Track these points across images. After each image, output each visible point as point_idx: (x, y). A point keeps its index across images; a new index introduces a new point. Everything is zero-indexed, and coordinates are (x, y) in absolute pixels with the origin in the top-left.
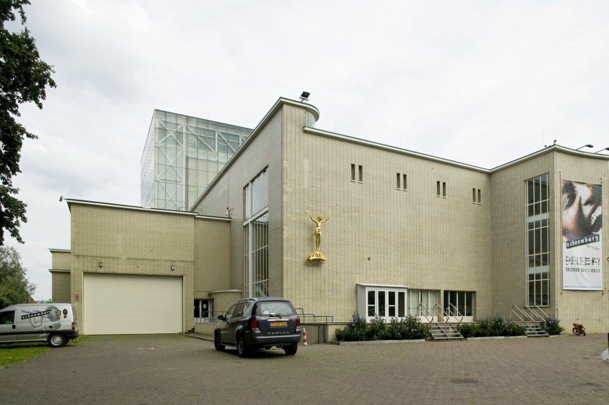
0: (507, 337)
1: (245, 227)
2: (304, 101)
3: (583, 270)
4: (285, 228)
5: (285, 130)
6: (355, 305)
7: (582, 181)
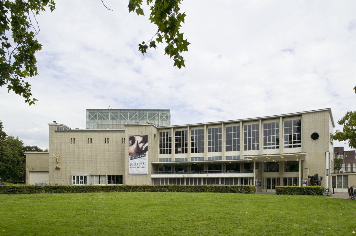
7: (138, 135)
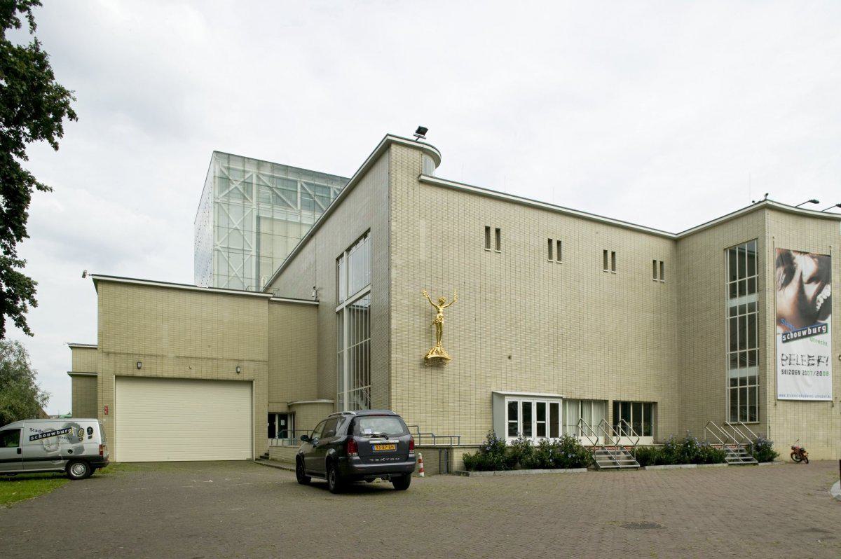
0: (700, 466)
1: (338, 313)
2: (420, 140)
3: (805, 373)
4: (393, 314)
5: (393, 180)
6: (490, 421)
7: (803, 250)
